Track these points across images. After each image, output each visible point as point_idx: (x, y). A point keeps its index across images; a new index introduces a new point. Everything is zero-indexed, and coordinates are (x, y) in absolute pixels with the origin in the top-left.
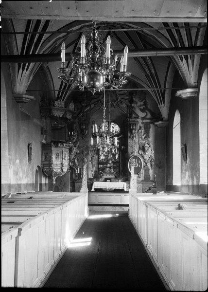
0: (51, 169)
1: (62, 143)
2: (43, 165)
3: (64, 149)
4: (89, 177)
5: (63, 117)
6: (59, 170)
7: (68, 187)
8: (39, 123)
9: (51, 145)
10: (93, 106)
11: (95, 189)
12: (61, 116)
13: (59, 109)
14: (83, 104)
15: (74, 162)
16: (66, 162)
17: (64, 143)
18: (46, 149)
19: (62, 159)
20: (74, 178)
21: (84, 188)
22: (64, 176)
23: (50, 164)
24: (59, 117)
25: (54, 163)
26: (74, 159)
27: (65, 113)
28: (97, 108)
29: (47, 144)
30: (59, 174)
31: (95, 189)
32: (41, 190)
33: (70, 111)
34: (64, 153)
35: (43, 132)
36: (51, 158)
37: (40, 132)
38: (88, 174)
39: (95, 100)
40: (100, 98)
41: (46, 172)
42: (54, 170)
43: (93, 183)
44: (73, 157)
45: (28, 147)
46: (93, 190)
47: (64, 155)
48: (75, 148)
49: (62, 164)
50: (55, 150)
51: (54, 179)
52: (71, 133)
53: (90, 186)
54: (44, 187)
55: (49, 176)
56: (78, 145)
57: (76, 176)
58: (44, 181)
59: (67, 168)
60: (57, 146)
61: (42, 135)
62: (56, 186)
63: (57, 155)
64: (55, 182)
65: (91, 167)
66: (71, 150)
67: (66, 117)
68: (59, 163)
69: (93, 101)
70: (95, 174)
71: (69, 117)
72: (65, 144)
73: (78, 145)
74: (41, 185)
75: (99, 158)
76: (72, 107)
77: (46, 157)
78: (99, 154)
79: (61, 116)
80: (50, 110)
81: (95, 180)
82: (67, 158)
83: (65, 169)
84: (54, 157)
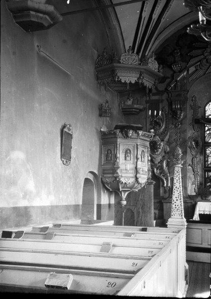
0: (116, 178)
1: (136, 129)
2: (104, 172)
3: (139, 142)
4: (189, 193)
5: (137, 83)
6: (131, 181)
7: (150, 213)
8: (96, 97)
9: (115, 133)
10: (192, 69)
11: (200, 215)
12: (133, 82)
13: (130, 69)
14: (175, 68)
15: (161, 168)
16: (144, 166)
17: (140, 129)
18: (107, 142)
19: (137, 159)
20: (161, 195)
21: (177, 218)
22: (143, 190)
23: (114, 170)
24: (130, 83)
25: (122, 167)
26: (161, 162)
27: (141, 75)
28: (201, 72)
29: (110, 133)
30: (131, 188)
31: (200, 215)
32: (99, 217)
33: (151, 73)
34: (140, 149)
35: (102, 112)
36: (116, 157)
37: (97, 113)
38: (185, 188)
39: (197, 59)
40: (206, 54)
41: (108, 184)
42: (122, 180)
43: (196, 204)
44: (159, 159)
45: (62, 131)
46: (196, 217)
47: (140, 153)
48: (162, 144)
49: (136, 168)
50: (122, 145)
51: (124, 196)
52: (153, 113)
53: (189, 212)
54: (105, 212)
55: (114, 189)
56: (167, 137)
57: (165, 192)
58: (106, 199)
59: (146, 177)
60: (126, 136)
61: (102, 119)
62: (128, 210)
63: (127, 152)
64: (124, 203)
65: (192, 176)
66: (153, 147)
67: (142, 84)
68: (130, 166)
69: (192, 62)
70: (199, 189)
71: (148, 83)
72: (141, 133)
73: (167, 137)
74: (99, 206)
75: (206, 161)
76: (153, 65)
77: (107, 156)
78: (205, 153)
79: (133, 82)
80: (113, 72)
81: (199, 198)
82: (147, 157)
83: (143, 179)
84: (121, 156)
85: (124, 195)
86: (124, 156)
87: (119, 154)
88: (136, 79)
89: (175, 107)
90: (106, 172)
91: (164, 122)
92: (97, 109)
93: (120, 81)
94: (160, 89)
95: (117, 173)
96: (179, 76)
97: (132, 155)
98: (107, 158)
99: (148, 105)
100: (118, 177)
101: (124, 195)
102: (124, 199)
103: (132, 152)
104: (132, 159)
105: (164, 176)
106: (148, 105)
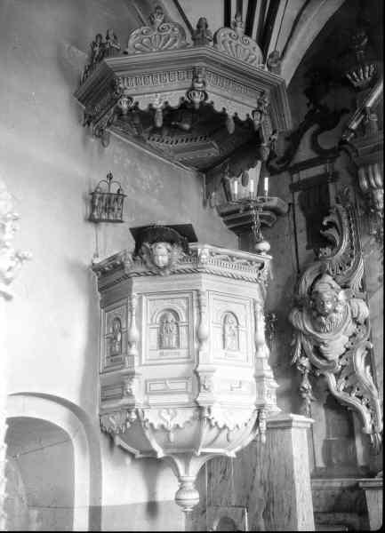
12: (243, 118)
24: (236, 118)
42: (152, 417)
79: (174, 103)
85: (186, 471)
86: (154, 334)
87: (140, 329)
88: (183, 93)
89: (369, 183)
90: (153, 387)
91: (346, 230)
92: (81, 200)
93: (136, 107)
94: (326, 147)
95: (130, 395)
96: (368, 97)
97: (183, 330)
98: (161, 339)
99: (297, 194)
100: (134, 405)
101: (186, 471)
102: (190, 485)
103: (183, 318)
104: (184, 343)
105: (361, 398)
106: (297, 194)
